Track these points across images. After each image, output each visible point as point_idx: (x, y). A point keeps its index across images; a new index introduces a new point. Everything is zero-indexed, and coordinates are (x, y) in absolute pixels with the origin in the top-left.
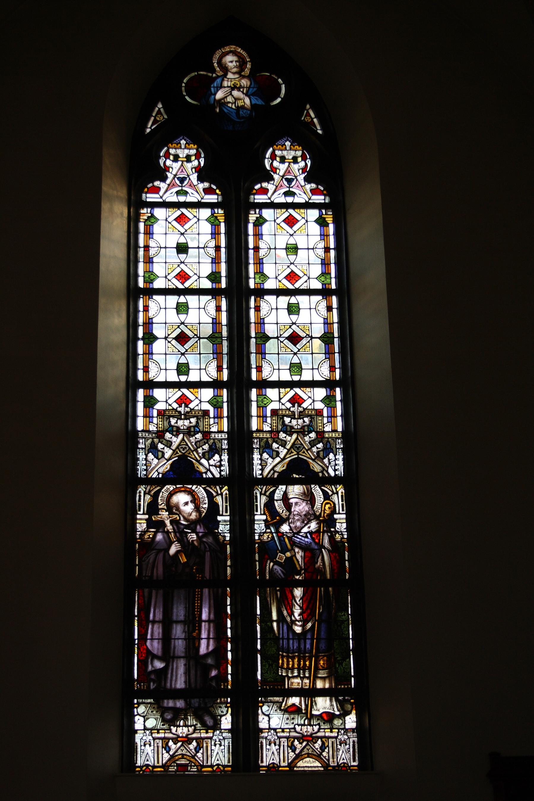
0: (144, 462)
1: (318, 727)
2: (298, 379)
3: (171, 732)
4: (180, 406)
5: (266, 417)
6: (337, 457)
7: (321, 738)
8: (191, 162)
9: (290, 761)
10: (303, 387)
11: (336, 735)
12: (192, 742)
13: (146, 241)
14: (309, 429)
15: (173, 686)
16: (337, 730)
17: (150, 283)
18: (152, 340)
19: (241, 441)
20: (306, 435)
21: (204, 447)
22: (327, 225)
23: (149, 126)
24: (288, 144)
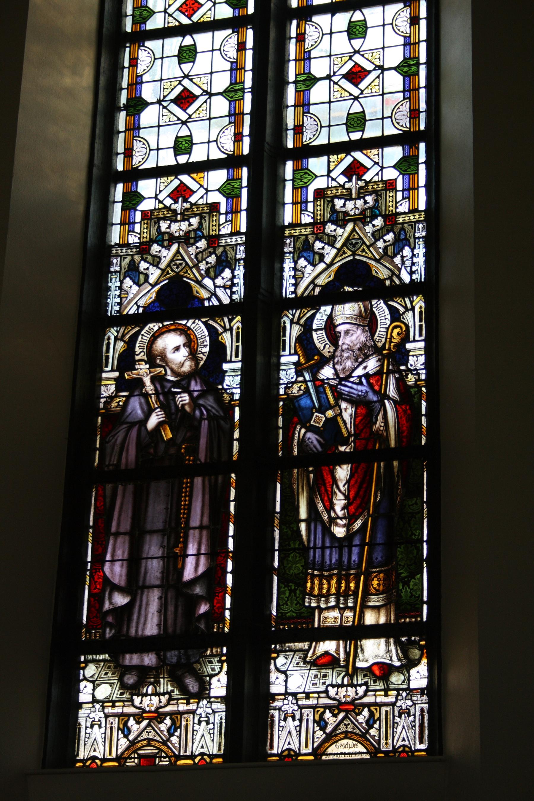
3: (328, 697)
6: (416, 252)
7: (368, 705)
9: (316, 745)
11: (394, 700)
12: (165, 719)
16: (395, 693)
19: (266, 243)
21: (209, 260)
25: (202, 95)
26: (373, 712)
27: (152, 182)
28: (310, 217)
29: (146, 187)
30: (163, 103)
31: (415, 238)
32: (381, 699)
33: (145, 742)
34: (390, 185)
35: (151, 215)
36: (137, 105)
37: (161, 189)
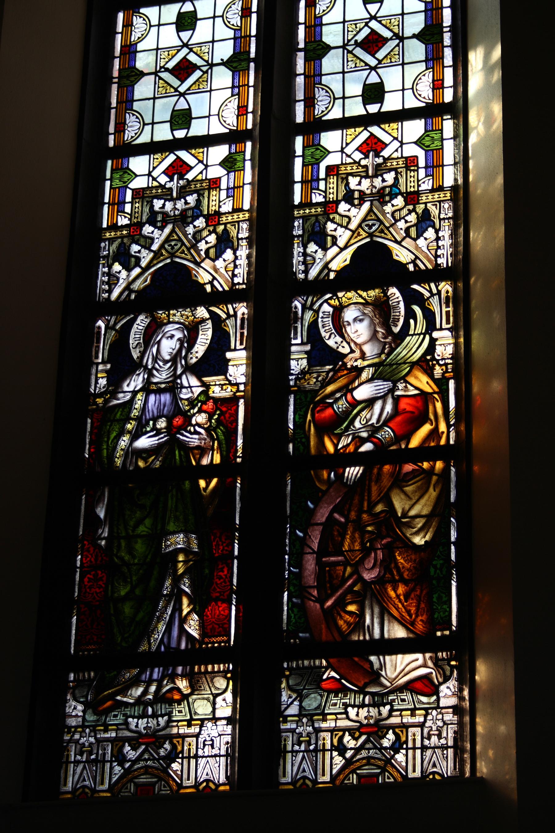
0: (106, 279)
2: (376, 111)
4: (367, 157)
7: (393, 727)
9: (334, 771)
10: (385, 123)
11: (422, 719)
12: (387, 733)
14: (391, 192)
15: (386, 636)
16: (423, 712)
18: (132, 79)
20: (386, 203)
21: (408, 218)
25: (391, 39)
26: (175, 744)
27: (337, 134)
28: (322, 196)
29: (330, 139)
30: (347, 47)
31: (238, 239)
33: (364, 761)
34: (215, 183)
35: (143, 194)
36: (132, 75)
37: (348, 142)
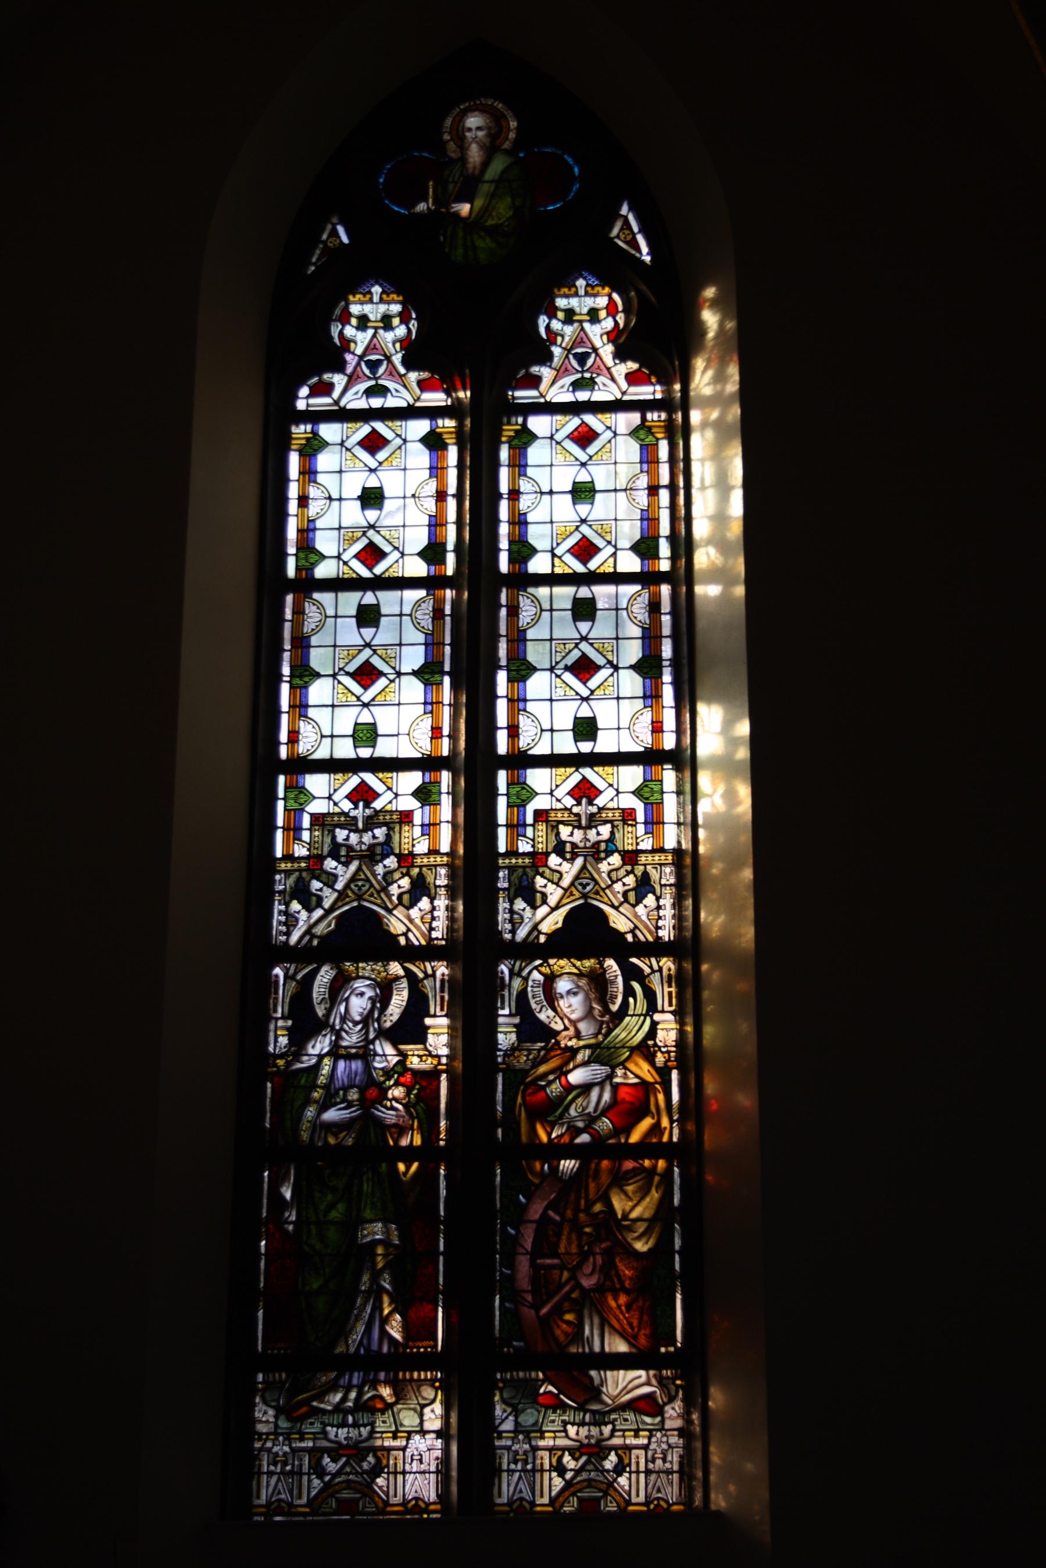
1: (368, 1428)
3: (567, 1436)
4: (579, 804)
5: (301, 829)
6: (662, 902)
7: (615, 1448)
8: (599, 321)
12: (609, 1454)
13: (513, 480)
15: (607, 1349)
17: (520, 563)
19: (477, 870)
20: (377, 862)
21: (626, 880)
22: (444, 447)
23: (314, 260)
24: (377, 290)
32: (631, 1441)
34: (406, 817)
